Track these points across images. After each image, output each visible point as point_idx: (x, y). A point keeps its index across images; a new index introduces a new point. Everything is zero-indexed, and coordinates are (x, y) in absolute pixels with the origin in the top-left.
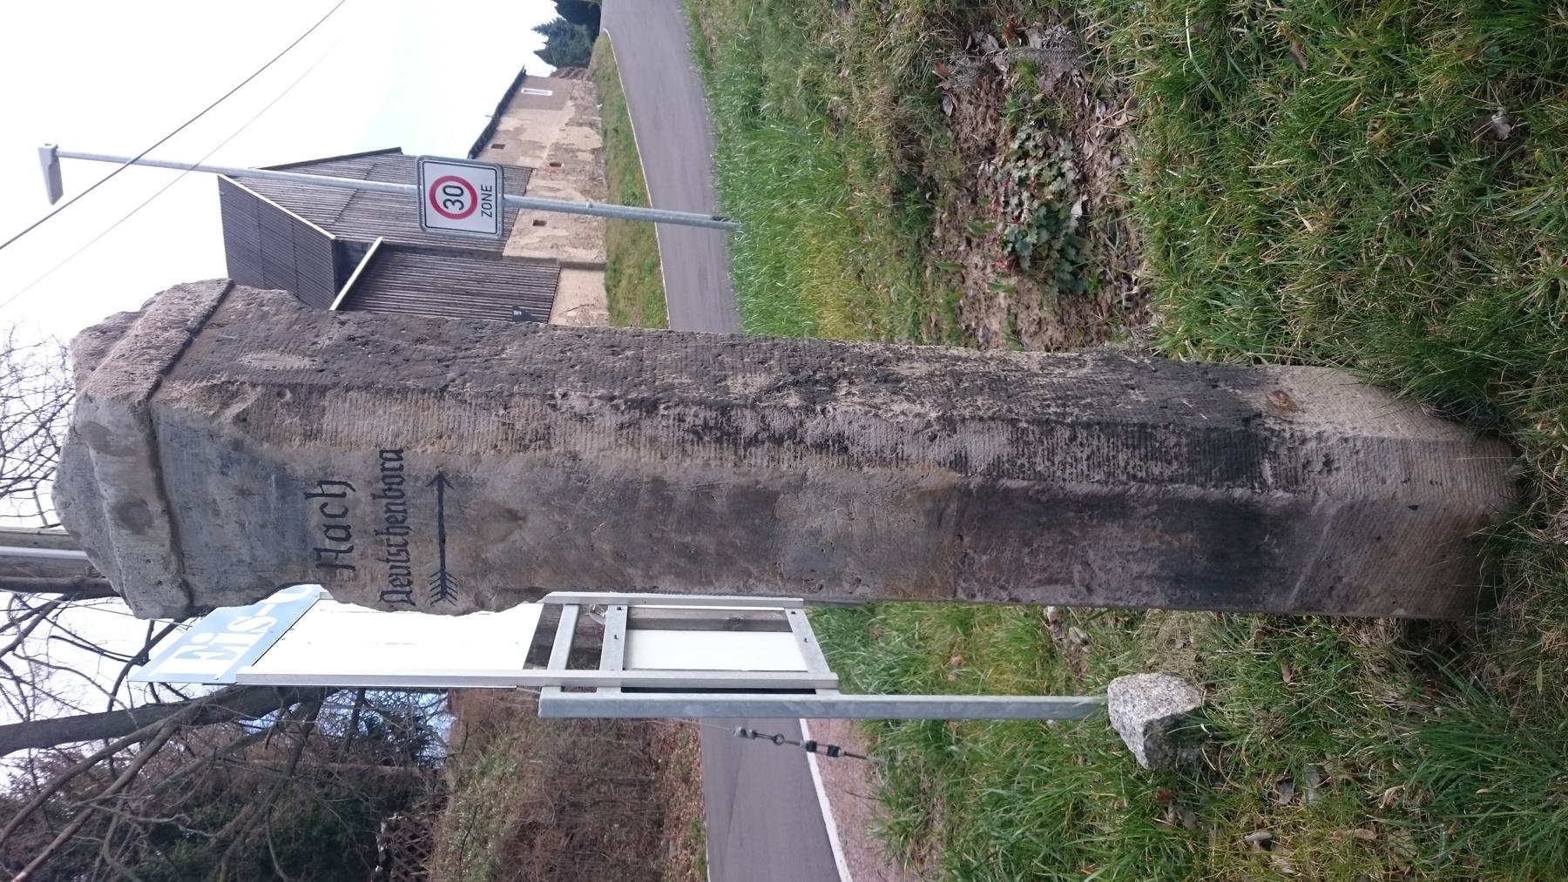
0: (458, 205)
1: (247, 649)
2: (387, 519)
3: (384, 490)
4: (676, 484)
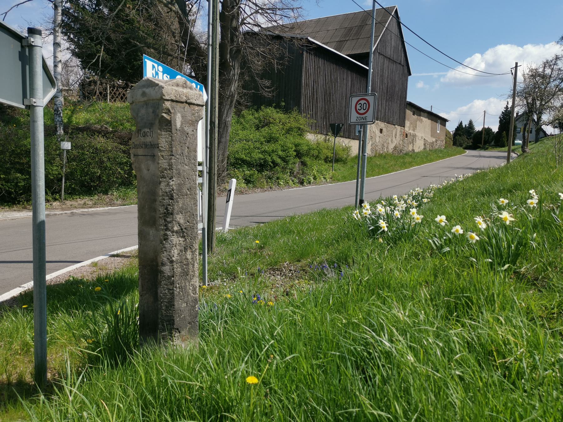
0: (360, 108)
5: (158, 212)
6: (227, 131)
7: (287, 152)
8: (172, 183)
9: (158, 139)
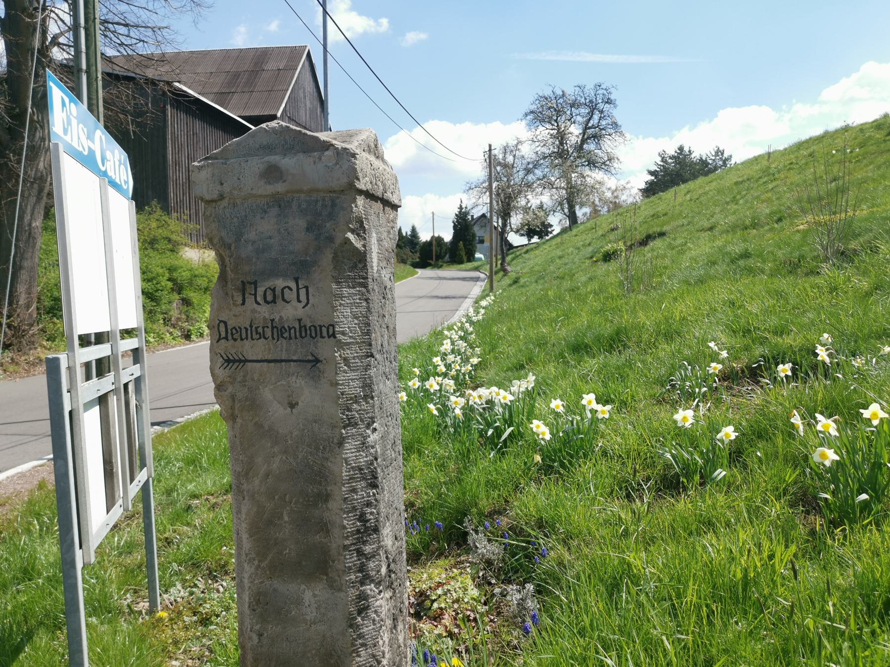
1: (70, 142)
2: (284, 327)
3: (305, 326)
4: (327, 508)
5: (336, 532)
6: (34, 244)
7: (155, 282)
8: (373, 438)
9: (333, 309)
